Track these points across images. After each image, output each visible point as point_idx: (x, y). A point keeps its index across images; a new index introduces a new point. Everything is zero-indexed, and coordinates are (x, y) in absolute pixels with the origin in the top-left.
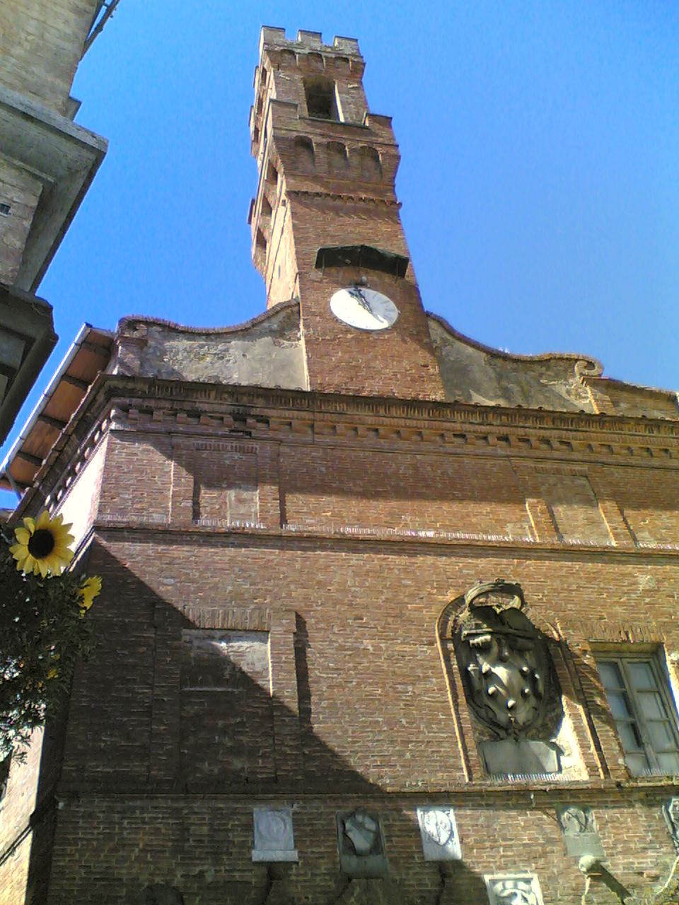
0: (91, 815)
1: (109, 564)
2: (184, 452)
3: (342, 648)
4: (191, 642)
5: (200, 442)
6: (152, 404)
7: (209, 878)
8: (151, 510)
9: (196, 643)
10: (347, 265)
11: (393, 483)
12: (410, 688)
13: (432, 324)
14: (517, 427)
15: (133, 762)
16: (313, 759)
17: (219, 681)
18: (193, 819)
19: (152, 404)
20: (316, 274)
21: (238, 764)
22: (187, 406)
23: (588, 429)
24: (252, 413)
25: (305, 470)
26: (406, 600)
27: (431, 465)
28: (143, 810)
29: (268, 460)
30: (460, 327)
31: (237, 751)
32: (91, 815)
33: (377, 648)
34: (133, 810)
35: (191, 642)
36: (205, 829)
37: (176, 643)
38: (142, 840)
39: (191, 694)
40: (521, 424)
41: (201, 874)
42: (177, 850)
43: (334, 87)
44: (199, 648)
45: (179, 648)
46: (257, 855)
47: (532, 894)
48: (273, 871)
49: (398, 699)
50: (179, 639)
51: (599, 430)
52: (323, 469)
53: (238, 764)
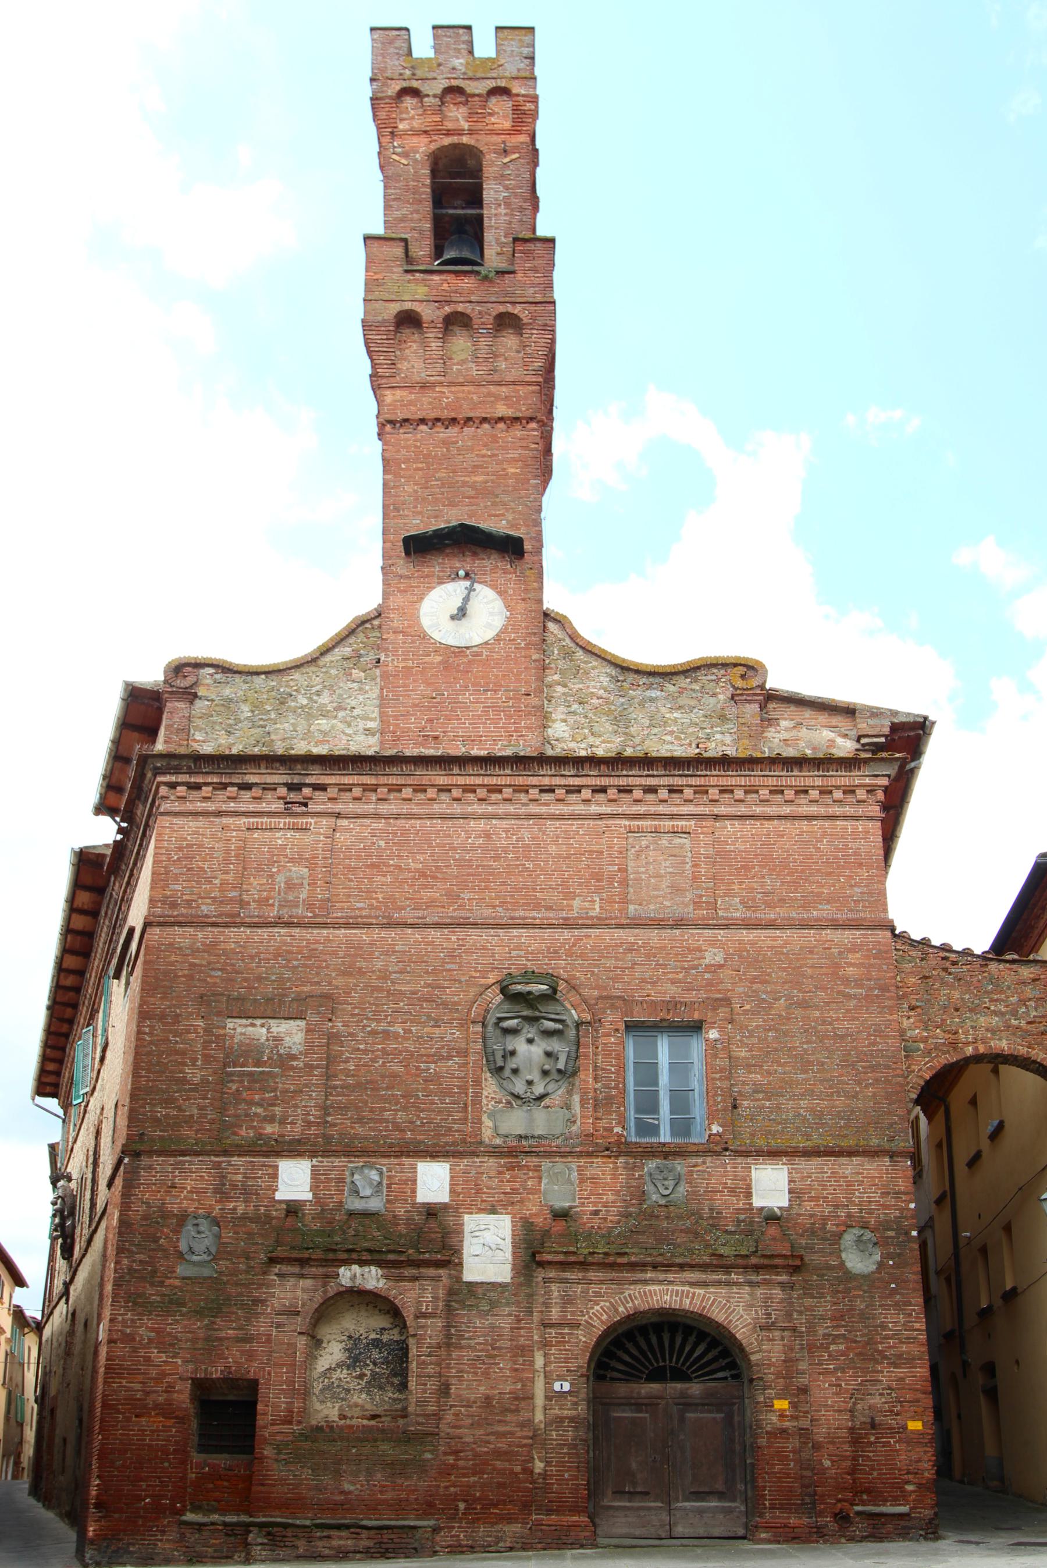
0: (150, 1167)
2: (234, 834)
3: (373, 1033)
4: (235, 1029)
5: (251, 820)
8: (200, 901)
9: (239, 1030)
10: (447, 546)
11: (457, 856)
14: (543, 775)
16: (335, 1125)
17: (258, 1063)
20: (402, 566)
21: (269, 1129)
24: (307, 782)
26: (446, 983)
27: (506, 831)
29: (322, 838)
30: (587, 631)
33: (408, 1031)
35: (235, 1029)
36: (240, 1177)
37: (222, 1032)
38: (189, 1184)
40: (625, 773)
42: (216, 1191)
43: (452, 215)
44: (242, 1034)
45: (225, 1035)
46: (278, 1196)
47: (114, 781)
48: (293, 1209)
49: (418, 1076)
50: (225, 1027)
51: (458, 772)
52: (382, 843)
53: (269, 1129)
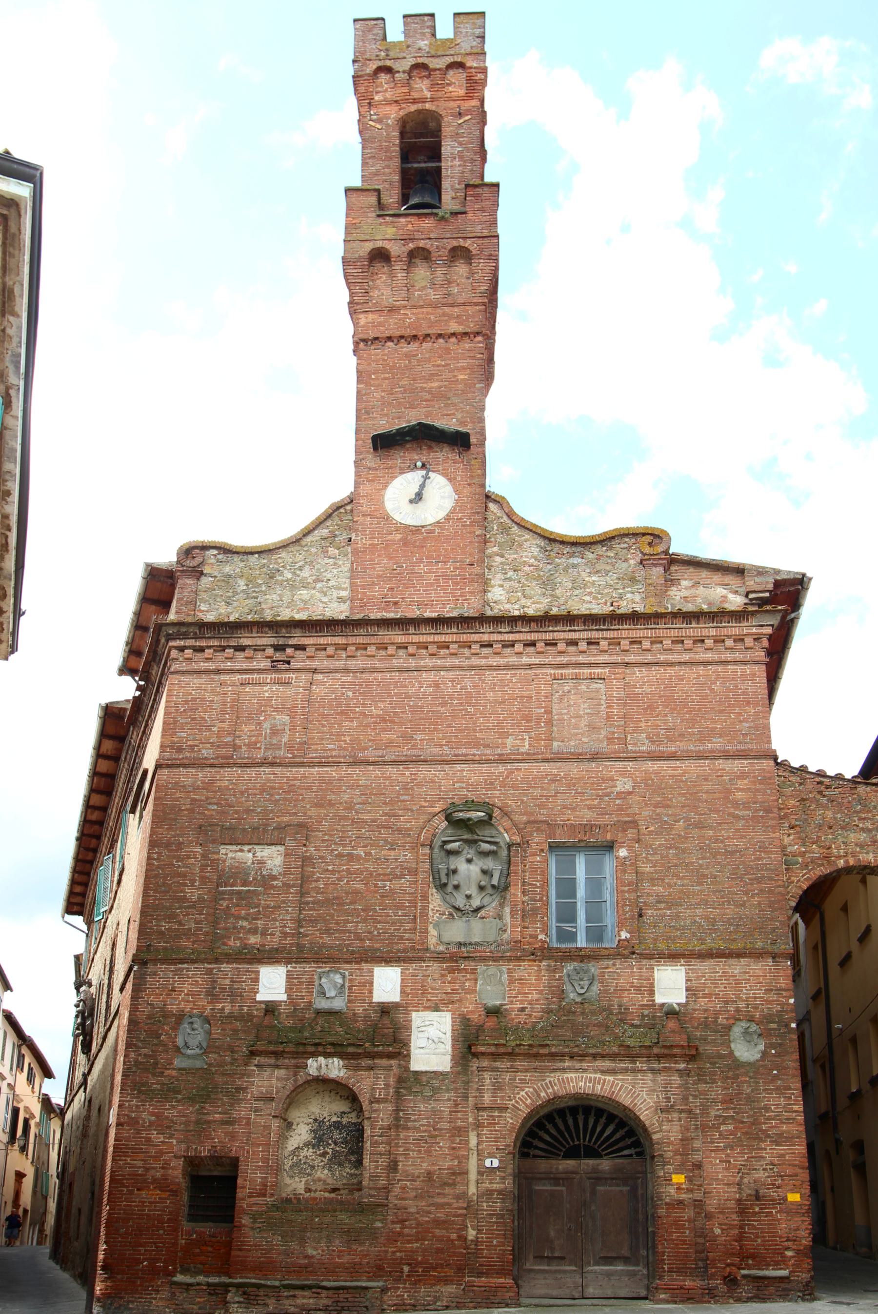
1: (385, 379)
2: (230, 688)
3: (340, 855)
5: (244, 677)
6: (203, 643)
7: (227, 1011)
9: (230, 855)
12: (388, 883)
13: (491, 506)
15: (634, 1062)
18: (220, 975)
19: (203, 643)
20: (371, 460)
21: (253, 940)
22: (233, 643)
23: (621, 627)
25: (333, 696)
27: (452, 681)
28: (188, 970)
29: (301, 690)
31: (254, 931)
32: (155, 974)
33: (368, 854)
34: (182, 969)
35: (226, 854)
36: (227, 982)
37: (216, 857)
38: (186, 988)
39: (224, 893)
41: (223, 1009)
44: (232, 858)
48: (271, 1008)
